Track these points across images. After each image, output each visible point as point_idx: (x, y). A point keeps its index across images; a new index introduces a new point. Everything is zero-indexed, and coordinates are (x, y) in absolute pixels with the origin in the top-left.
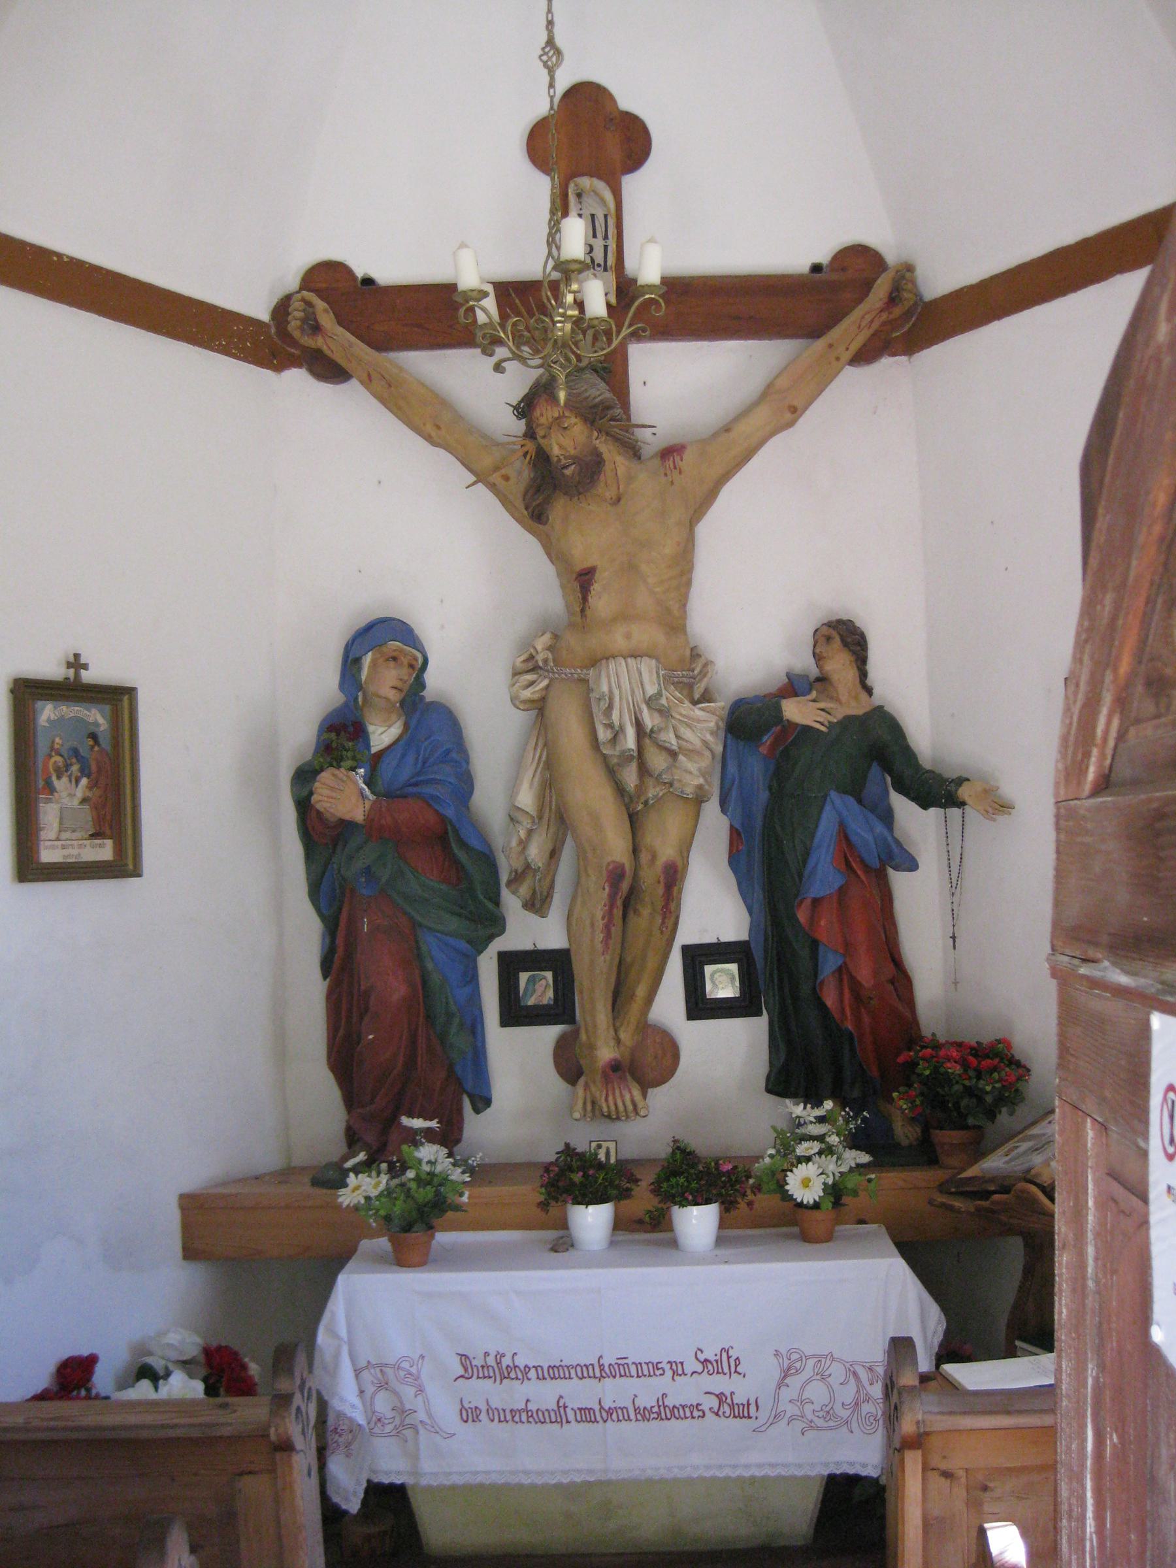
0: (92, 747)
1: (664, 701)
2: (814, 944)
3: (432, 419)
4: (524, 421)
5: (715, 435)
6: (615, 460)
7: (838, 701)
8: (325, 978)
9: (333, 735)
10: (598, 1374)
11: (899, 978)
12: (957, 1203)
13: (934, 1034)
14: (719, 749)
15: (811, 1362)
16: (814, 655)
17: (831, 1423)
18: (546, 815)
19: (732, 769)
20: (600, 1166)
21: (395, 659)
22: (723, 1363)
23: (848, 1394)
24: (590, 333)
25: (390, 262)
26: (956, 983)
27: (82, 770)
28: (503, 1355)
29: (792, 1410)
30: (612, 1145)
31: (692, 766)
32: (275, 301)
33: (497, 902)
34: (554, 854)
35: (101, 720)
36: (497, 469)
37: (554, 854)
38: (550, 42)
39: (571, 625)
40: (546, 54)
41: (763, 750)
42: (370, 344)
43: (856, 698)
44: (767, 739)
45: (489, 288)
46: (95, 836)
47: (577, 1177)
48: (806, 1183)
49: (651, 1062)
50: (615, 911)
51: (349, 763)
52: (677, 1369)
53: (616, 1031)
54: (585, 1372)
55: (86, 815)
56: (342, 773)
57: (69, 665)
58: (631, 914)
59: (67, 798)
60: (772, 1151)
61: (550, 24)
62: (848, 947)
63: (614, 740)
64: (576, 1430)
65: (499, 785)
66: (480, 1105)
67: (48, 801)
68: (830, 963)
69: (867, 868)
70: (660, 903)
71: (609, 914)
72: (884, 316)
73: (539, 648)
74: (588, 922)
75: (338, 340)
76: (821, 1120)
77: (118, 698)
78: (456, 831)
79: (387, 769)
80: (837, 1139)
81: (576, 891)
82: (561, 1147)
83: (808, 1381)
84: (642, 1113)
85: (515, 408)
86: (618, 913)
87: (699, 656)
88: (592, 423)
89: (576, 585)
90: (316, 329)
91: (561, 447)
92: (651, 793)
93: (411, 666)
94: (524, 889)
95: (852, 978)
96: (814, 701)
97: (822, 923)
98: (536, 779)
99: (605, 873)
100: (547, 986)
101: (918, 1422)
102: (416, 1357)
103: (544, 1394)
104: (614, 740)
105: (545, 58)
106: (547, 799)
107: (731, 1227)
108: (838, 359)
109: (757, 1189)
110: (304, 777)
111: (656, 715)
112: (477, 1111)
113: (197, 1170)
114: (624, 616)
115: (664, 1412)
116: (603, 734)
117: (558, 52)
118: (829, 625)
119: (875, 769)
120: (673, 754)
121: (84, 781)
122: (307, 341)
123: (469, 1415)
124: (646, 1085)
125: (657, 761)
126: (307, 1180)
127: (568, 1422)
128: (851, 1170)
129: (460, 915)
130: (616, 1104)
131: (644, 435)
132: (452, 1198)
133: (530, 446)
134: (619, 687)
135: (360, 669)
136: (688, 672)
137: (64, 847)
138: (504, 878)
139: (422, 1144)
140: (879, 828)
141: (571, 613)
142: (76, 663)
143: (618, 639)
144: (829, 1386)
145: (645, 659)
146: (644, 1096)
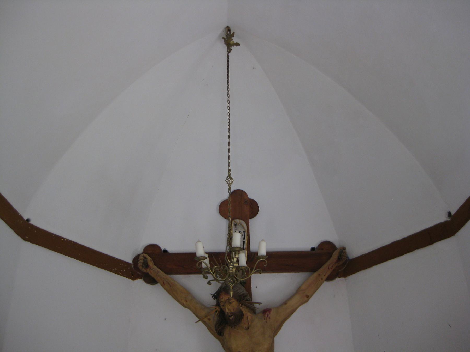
3: (184, 298)
4: (216, 300)
5: (281, 305)
6: (248, 314)
24: (241, 271)
25: (172, 244)
32: (134, 256)
36: (206, 317)
38: (229, 176)
40: (228, 179)
42: (165, 273)
45: (207, 256)
61: (229, 170)
72: (337, 264)
75: (154, 270)
85: (213, 295)
88: (240, 301)
90: (147, 266)
91: (229, 309)
105: (227, 181)
108: (322, 279)
117: (232, 179)
122: (144, 270)
131: (257, 306)
133: (218, 309)
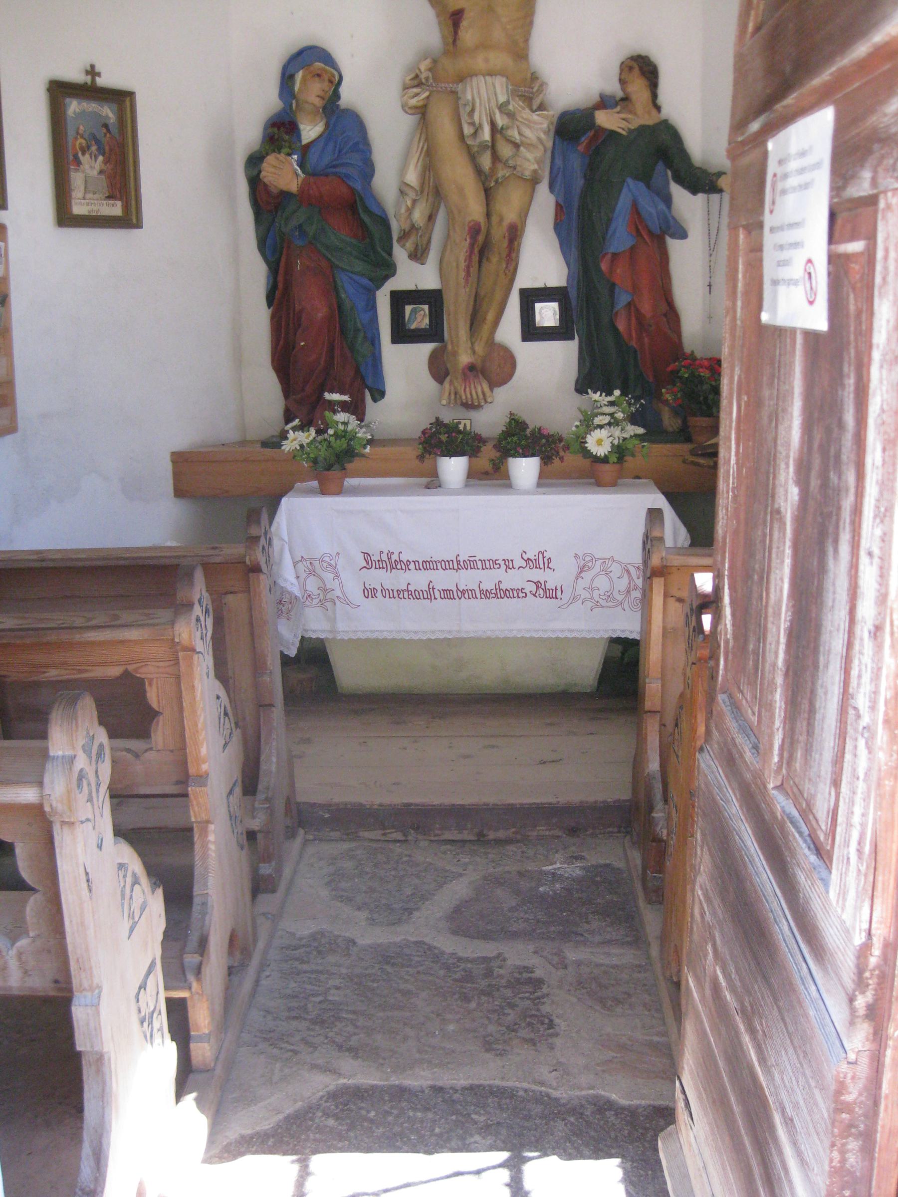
0: (105, 135)
1: (511, 107)
2: (613, 286)
7: (635, 114)
8: (269, 308)
9: (275, 130)
10: (456, 567)
11: (671, 314)
12: (702, 461)
13: (693, 352)
14: (549, 145)
15: (599, 563)
16: (620, 80)
17: (610, 604)
18: (426, 189)
19: (559, 162)
20: (460, 432)
21: (319, 75)
22: (540, 561)
23: (623, 583)
26: (710, 317)
27: (99, 149)
28: (392, 553)
29: (585, 594)
30: (468, 422)
31: (529, 156)
33: (390, 254)
34: (431, 218)
35: (111, 115)
37: (431, 218)
39: (446, 53)
41: (581, 148)
43: (649, 113)
44: (584, 140)
46: (109, 197)
47: (444, 438)
48: (600, 442)
49: (497, 368)
50: (473, 257)
51: (286, 150)
52: (509, 565)
53: (472, 344)
54: (446, 565)
55: (103, 181)
56: (282, 156)
57: (87, 73)
58: (484, 260)
59: (91, 167)
60: (578, 423)
62: (635, 289)
63: (475, 134)
64: (440, 603)
65: (392, 171)
66: (378, 397)
67: (77, 170)
68: (623, 299)
69: (651, 234)
70: (504, 253)
71: (469, 258)
74: (455, 264)
76: (612, 404)
77: (122, 99)
78: (361, 199)
79: (313, 157)
80: (622, 415)
81: (447, 241)
82: (433, 420)
83: (597, 575)
84: (489, 400)
86: (475, 258)
87: (537, 78)
89: (450, 23)
92: (500, 174)
93: (331, 82)
94: (410, 244)
95: (637, 310)
96: (618, 113)
97: (618, 271)
98: (419, 164)
99: (467, 228)
100: (424, 315)
102: (334, 554)
103: (419, 580)
104: (475, 134)
106: (427, 178)
107: (547, 478)
109: (567, 448)
110: (254, 161)
111: (505, 117)
112: (375, 400)
113: (183, 438)
114: (484, 45)
115: (500, 593)
116: (467, 130)
119: (660, 166)
120: (517, 146)
121: (101, 158)
123: (370, 593)
124: (493, 385)
125: (505, 151)
127: (435, 598)
128: (631, 437)
129: (365, 261)
130: (471, 395)
132: (358, 449)
135: (293, 84)
136: (529, 88)
137: (88, 204)
138: (395, 237)
139: (339, 412)
140: (662, 206)
141: (445, 43)
142: (92, 72)
143: (479, 62)
144: (610, 579)
145: (499, 77)
146: (491, 390)
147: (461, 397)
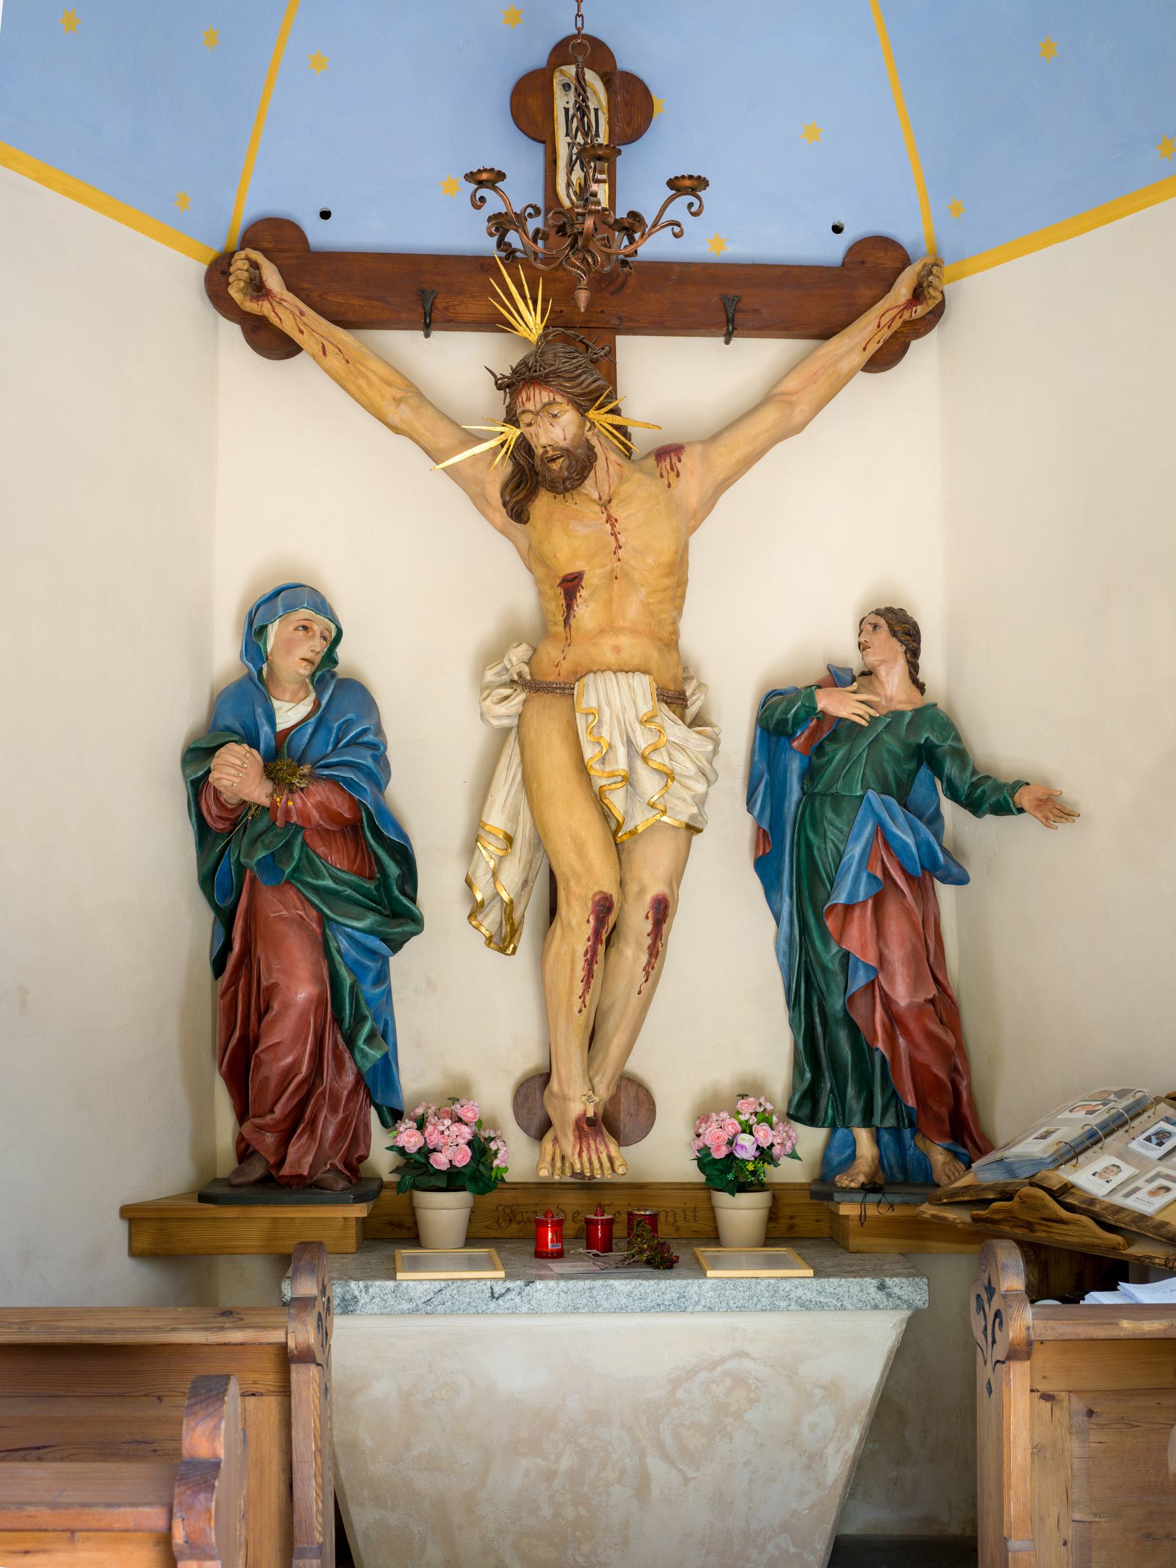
6: (607, 460)
73: (514, 660)
99: (590, 904)
101: (1028, 1328)
114: (609, 628)
116: (589, 752)
118: (878, 613)
119: (924, 772)
122: (251, 306)
126: (608, 886)
134: (609, 704)
140: (926, 832)
145: (638, 675)
147: (572, 1166)
